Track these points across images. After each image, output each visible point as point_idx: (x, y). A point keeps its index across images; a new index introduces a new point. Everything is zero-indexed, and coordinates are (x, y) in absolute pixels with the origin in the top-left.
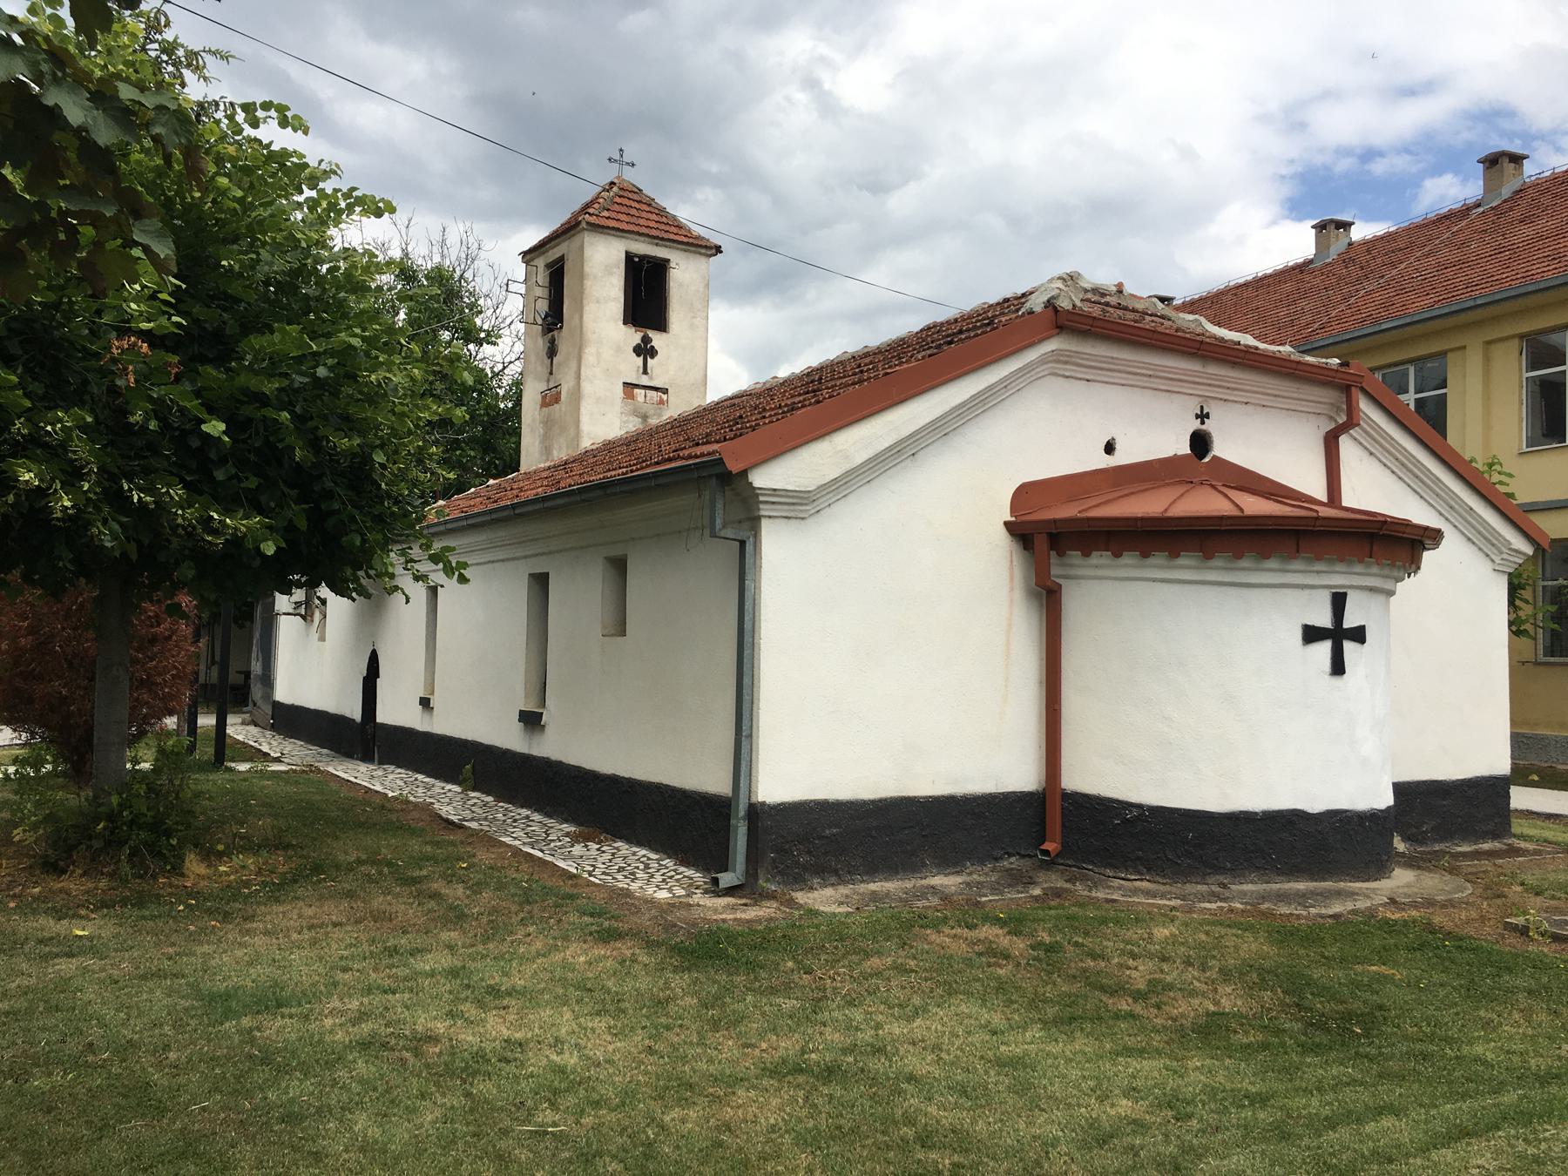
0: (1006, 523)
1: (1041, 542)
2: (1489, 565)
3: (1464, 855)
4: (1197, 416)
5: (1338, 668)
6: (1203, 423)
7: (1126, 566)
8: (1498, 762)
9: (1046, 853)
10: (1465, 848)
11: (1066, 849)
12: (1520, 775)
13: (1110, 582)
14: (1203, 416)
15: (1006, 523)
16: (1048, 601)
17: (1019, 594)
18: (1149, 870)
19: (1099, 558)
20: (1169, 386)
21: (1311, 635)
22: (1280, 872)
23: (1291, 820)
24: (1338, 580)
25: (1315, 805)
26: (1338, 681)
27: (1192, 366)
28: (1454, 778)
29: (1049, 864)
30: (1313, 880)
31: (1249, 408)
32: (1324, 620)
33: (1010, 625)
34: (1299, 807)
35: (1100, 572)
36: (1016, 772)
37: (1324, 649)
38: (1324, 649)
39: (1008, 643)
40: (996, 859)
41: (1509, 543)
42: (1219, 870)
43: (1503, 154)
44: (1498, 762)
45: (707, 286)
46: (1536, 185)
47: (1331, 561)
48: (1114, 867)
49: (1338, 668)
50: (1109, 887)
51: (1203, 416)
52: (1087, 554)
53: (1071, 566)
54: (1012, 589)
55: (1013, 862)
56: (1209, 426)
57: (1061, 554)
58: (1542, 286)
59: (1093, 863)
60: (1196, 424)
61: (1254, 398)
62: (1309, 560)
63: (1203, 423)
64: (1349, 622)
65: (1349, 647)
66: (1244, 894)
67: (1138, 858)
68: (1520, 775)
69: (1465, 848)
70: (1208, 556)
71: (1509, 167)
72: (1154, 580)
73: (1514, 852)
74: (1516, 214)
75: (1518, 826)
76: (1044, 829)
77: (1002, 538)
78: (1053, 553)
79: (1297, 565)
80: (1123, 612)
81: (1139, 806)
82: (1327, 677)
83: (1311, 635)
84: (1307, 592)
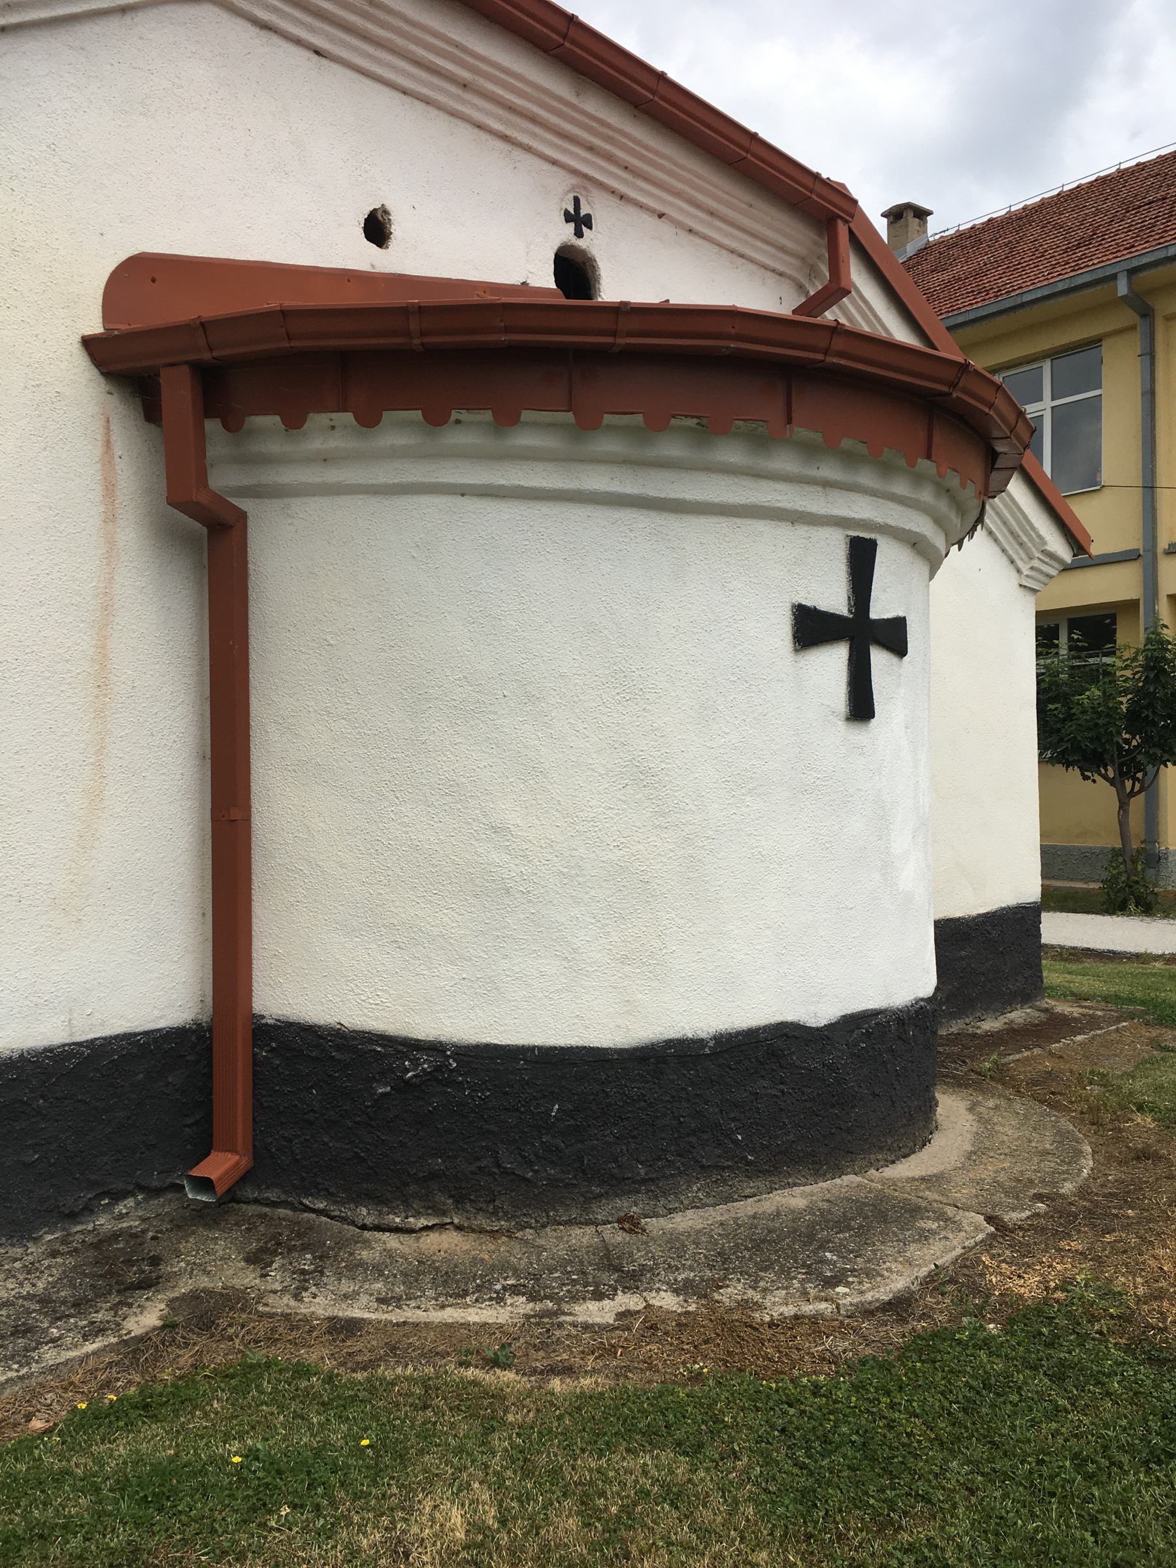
0: (88, 343)
1: (178, 391)
2: (1013, 579)
3: (994, 1040)
4: (568, 217)
5: (861, 706)
6: (579, 234)
7: (394, 454)
8: (1022, 883)
9: (205, 1184)
10: (991, 1025)
11: (261, 1171)
12: (1056, 899)
13: (359, 500)
14: (579, 221)
15: (88, 343)
16: (212, 547)
17: (131, 535)
18: (459, 1201)
19: (329, 432)
20: (510, 127)
21: (811, 628)
22: (755, 1171)
23: (771, 1049)
24: (862, 509)
25: (819, 1009)
26: (860, 735)
27: (553, 83)
28: (974, 912)
29: (223, 1207)
30: (819, 1174)
31: (663, 227)
32: (834, 599)
33: (106, 608)
34: (790, 1018)
35: (333, 475)
36: (124, 977)
37: (833, 661)
38: (833, 661)
39: (102, 656)
40: (73, 1217)
41: (1044, 543)
42: (619, 1184)
43: (909, 207)
44: (1022, 883)
45: (108, 422)
46: (939, 243)
47: (850, 459)
48: (377, 1199)
49: (861, 706)
50: (355, 1268)
51: (579, 221)
52: (294, 423)
53: (266, 460)
54: (110, 518)
55: (126, 1215)
56: (593, 243)
57: (233, 425)
58: (972, 316)
59: (329, 1195)
60: (566, 232)
61: (676, 208)
62: (809, 451)
63: (579, 234)
64: (881, 608)
65: (879, 658)
66: (676, 1244)
67: (434, 1176)
68: (1056, 899)
69: (991, 1025)
70: (587, 424)
71: (914, 222)
72: (463, 491)
73: (1058, 1026)
74: (925, 266)
75: (1052, 974)
76: (208, 1118)
77: (78, 386)
78: (212, 426)
79: (785, 461)
80: (388, 557)
81: (435, 1048)
82: (842, 725)
83: (811, 628)
84: (802, 530)
